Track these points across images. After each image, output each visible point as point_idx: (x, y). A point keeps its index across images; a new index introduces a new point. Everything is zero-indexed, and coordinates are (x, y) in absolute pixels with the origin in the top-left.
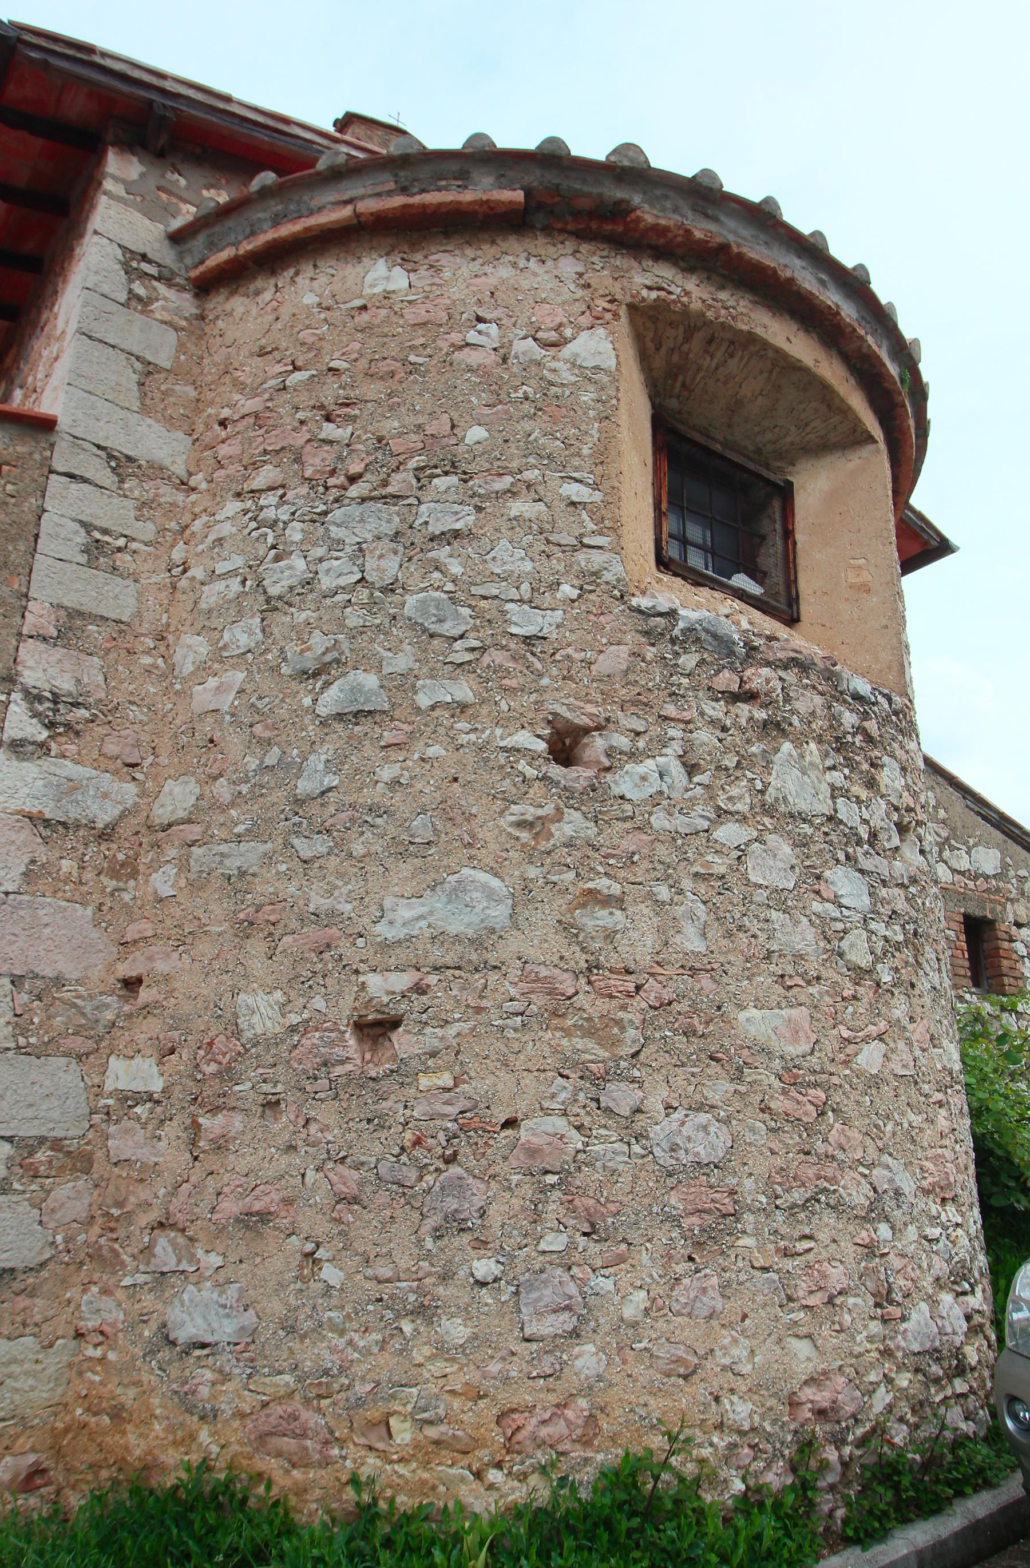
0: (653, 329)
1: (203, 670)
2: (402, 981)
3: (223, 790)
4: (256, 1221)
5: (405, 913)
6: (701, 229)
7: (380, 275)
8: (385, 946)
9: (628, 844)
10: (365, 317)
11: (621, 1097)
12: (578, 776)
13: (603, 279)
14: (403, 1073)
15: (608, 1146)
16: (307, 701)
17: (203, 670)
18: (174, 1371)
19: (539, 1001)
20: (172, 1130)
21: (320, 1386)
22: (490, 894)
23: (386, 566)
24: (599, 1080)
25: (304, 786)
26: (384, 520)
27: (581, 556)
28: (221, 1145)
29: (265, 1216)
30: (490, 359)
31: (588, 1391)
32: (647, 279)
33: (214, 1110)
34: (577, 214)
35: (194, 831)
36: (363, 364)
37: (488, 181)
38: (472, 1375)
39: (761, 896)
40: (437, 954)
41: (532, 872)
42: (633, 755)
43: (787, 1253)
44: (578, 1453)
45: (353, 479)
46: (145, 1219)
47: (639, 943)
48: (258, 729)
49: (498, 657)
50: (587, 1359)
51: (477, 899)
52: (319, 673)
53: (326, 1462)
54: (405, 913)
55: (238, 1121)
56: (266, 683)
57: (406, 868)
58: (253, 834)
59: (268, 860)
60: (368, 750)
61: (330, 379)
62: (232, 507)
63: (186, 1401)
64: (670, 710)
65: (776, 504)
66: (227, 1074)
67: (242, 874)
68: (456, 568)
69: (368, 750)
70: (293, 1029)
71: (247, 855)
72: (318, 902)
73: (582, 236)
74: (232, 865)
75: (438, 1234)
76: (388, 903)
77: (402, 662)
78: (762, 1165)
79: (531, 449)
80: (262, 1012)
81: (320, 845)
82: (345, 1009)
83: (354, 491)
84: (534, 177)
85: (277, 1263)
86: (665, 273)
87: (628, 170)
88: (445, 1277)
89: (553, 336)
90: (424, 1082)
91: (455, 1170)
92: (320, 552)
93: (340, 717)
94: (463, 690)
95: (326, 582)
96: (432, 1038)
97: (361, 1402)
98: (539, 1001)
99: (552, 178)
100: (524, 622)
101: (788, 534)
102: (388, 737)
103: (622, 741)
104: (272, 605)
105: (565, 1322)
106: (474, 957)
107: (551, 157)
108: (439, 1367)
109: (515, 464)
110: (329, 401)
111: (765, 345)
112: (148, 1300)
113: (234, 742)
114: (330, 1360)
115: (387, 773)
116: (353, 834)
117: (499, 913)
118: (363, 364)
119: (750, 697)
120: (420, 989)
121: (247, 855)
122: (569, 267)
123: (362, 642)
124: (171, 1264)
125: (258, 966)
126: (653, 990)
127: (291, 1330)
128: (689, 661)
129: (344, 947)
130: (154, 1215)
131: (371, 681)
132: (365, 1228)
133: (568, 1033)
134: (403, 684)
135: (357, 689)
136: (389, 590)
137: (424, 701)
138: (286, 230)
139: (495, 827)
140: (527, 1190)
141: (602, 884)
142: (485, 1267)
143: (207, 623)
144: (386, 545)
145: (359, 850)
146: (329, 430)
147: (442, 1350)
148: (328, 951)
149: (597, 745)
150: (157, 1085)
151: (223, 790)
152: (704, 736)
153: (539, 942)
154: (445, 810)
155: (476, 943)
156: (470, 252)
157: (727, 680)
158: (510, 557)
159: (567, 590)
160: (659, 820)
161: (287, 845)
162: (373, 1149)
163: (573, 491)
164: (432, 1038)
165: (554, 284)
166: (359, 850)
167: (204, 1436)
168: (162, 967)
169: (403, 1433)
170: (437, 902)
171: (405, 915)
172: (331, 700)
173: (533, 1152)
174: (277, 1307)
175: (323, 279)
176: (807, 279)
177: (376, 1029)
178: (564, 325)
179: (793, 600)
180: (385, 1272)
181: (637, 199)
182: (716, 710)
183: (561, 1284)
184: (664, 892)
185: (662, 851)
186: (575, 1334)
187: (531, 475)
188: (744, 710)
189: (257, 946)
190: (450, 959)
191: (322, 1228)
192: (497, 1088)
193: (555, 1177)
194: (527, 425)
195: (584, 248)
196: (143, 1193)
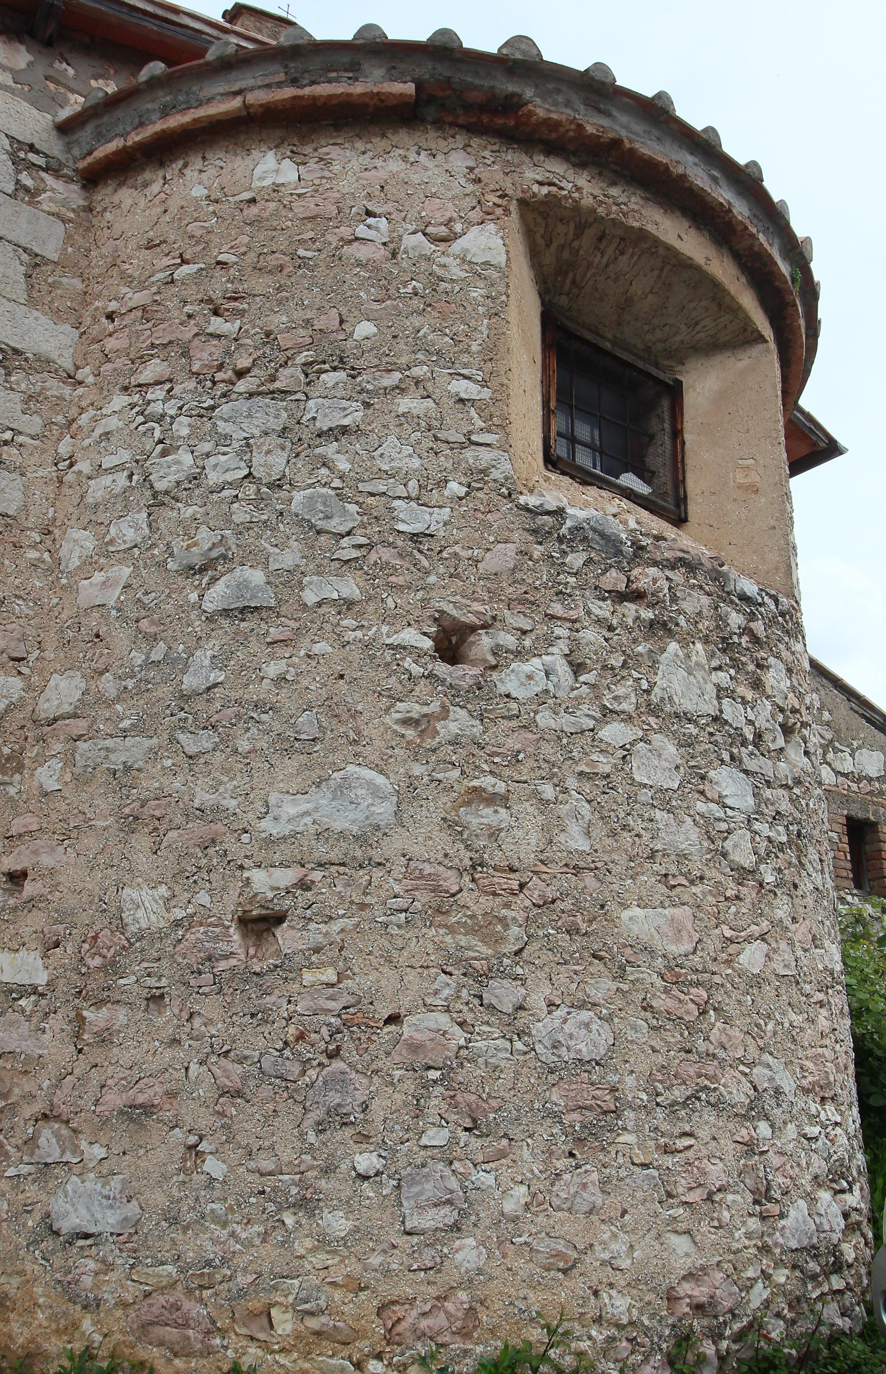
0: (545, 225)
1: (90, 565)
2: (287, 877)
3: (108, 685)
4: (138, 1114)
5: (290, 809)
6: (594, 125)
7: (269, 168)
8: (270, 842)
9: (513, 743)
10: (254, 210)
11: (504, 994)
12: (464, 674)
13: (494, 174)
14: (286, 968)
15: (490, 1043)
16: (194, 597)
17: (90, 565)
18: (57, 1261)
19: (423, 898)
20: (56, 1022)
21: (202, 1277)
22: (375, 791)
23: (273, 462)
24: (482, 977)
25: (190, 682)
26: (270, 415)
27: (469, 454)
28: (105, 1039)
29: (148, 1109)
30: (383, 252)
31: (468, 1284)
32: (538, 174)
33: (99, 1004)
34: (468, 108)
35: (79, 726)
36: (251, 257)
37: (378, 73)
38: (354, 1267)
39: (645, 796)
40: (322, 851)
41: (418, 770)
42: (520, 654)
43: (667, 1150)
44: (458, 1345)
45: (241, 374)
46: (29, 1110)
47: (524, 840)
48: (144, 624)
49: (385, 554)
50: (467, 1253)
51: (363, 795)
52: (205, 569)
53: (208, 1352)
54: (290, 809)
55: (122, 1015)
56: (151, 578)
57: (291, 765)
58: (138, 729)
59: (154, 754)
60: (254, 646)
61: (218, 272)
62: (120, 401)
63: (68, 1289)
64: (557, 609)
65: (665, 403)
66: (112, 968)
67: (127, 768)
68: (343, 465)
69: (254, 646)
70: (177, 923)
71: (133, 750)
72: (203, 797)
73: (473, 130)
74: (118, 759)
75: (320, 1128)
76: (273, 799)
77: (288, 558)
78: (643, 1063)
79: (419, 345)
80: (146, 907)
81: (206, 740)
82: (229, 905)
83: (242, 386)
84: (426, 69)
85: (161, 1154)
86: (556, 168)
87: (520, 62)
88: (327, 1171)
89: (443, 231)
90: (308, 977)
91: (338, 1065)
92: (207, 447)
93: (226, 613)
94: (349, 587)
95: (213, 478)
96: (316, 933)
97: (242, 1293)
98: (423, 898)
99: (443, 70)
100: (412, 519)
101: (677, 434)
102: (275, 633)
103: (508, 640)
104: (159, 501)
105: (447, 1215)
106: (360, 854)
107: (443, 49)
108: (321, 1259)
109: (403, 360)
110: (217, 295)
111: (656, 242)
112: (32, 1191)
113: (120, 638)
114: (212, 1251)
115: (273, 670)
116: (238, 730)
117: (384, 810)
118: (251, 257)
119: (637, 596)
120: (304, 885)
121: (133, 750)
122: (459, 161)
123: (249, 538)
124: (55, 1155)
125: (142, 860)
126: (537, 889)
127: (174, 1221)
128: (576, 560)
129: (229, 843)
130: (38, 1107)
131: (257, 577)
132: (248, 1121)
133: (451, 930)
134: (291, 580)
135: (243, 586)
136: (276, 486)
137: (310, 597)
138: (176, 121)
139: (381, 724)
140: (410, 1086)
141: (487, 782)
142: (367, 1161)
143: (94, 517)
144: (273, 440)
145: (244, 746)
146: (217, 324)
147: (323, 1242)
148: (212, 847)
149: (484, 642)
150: (41, 978)
151: (108, 685)
152: (591, 635)
153: (423, 839)
154: (331, 707)
155: (361, 839)
156: (360, 145)
157: (614, 579)
158: (398, 454)
159: (455, 488)
160: (545, 719)
161: (173, 740)
162: (257, 1043)
163: (462, 387)
164: (316, 933)
165: (444, 178)
166: (244, 746)
167: (87, 1325)
168: (46, 860)
169: (285, 1324)
170: (322, 799)
171: (291, 811)
172: (218, 595)
173: (415, 1048)
174: (159, 1198)
175: (211, 172)
176: (653, 148)
177: (260, 924)
178: (454, 221)
179: (681, 500)
180: (268, 1165)
181: (529, 93)
182: (602, 609)
183: (442, 1179)
184: (548, 791)
185: (547, 750)
186: (456, 1227)
187: (419, 371)
188: (630, 609)
189: (142, 841)
190: (335, 855)
191: (205, 1120)
192: (380, 983)
193: (436, 1073)
194: (416, 321)
195: (475, 142)
196: (27, 1085)
